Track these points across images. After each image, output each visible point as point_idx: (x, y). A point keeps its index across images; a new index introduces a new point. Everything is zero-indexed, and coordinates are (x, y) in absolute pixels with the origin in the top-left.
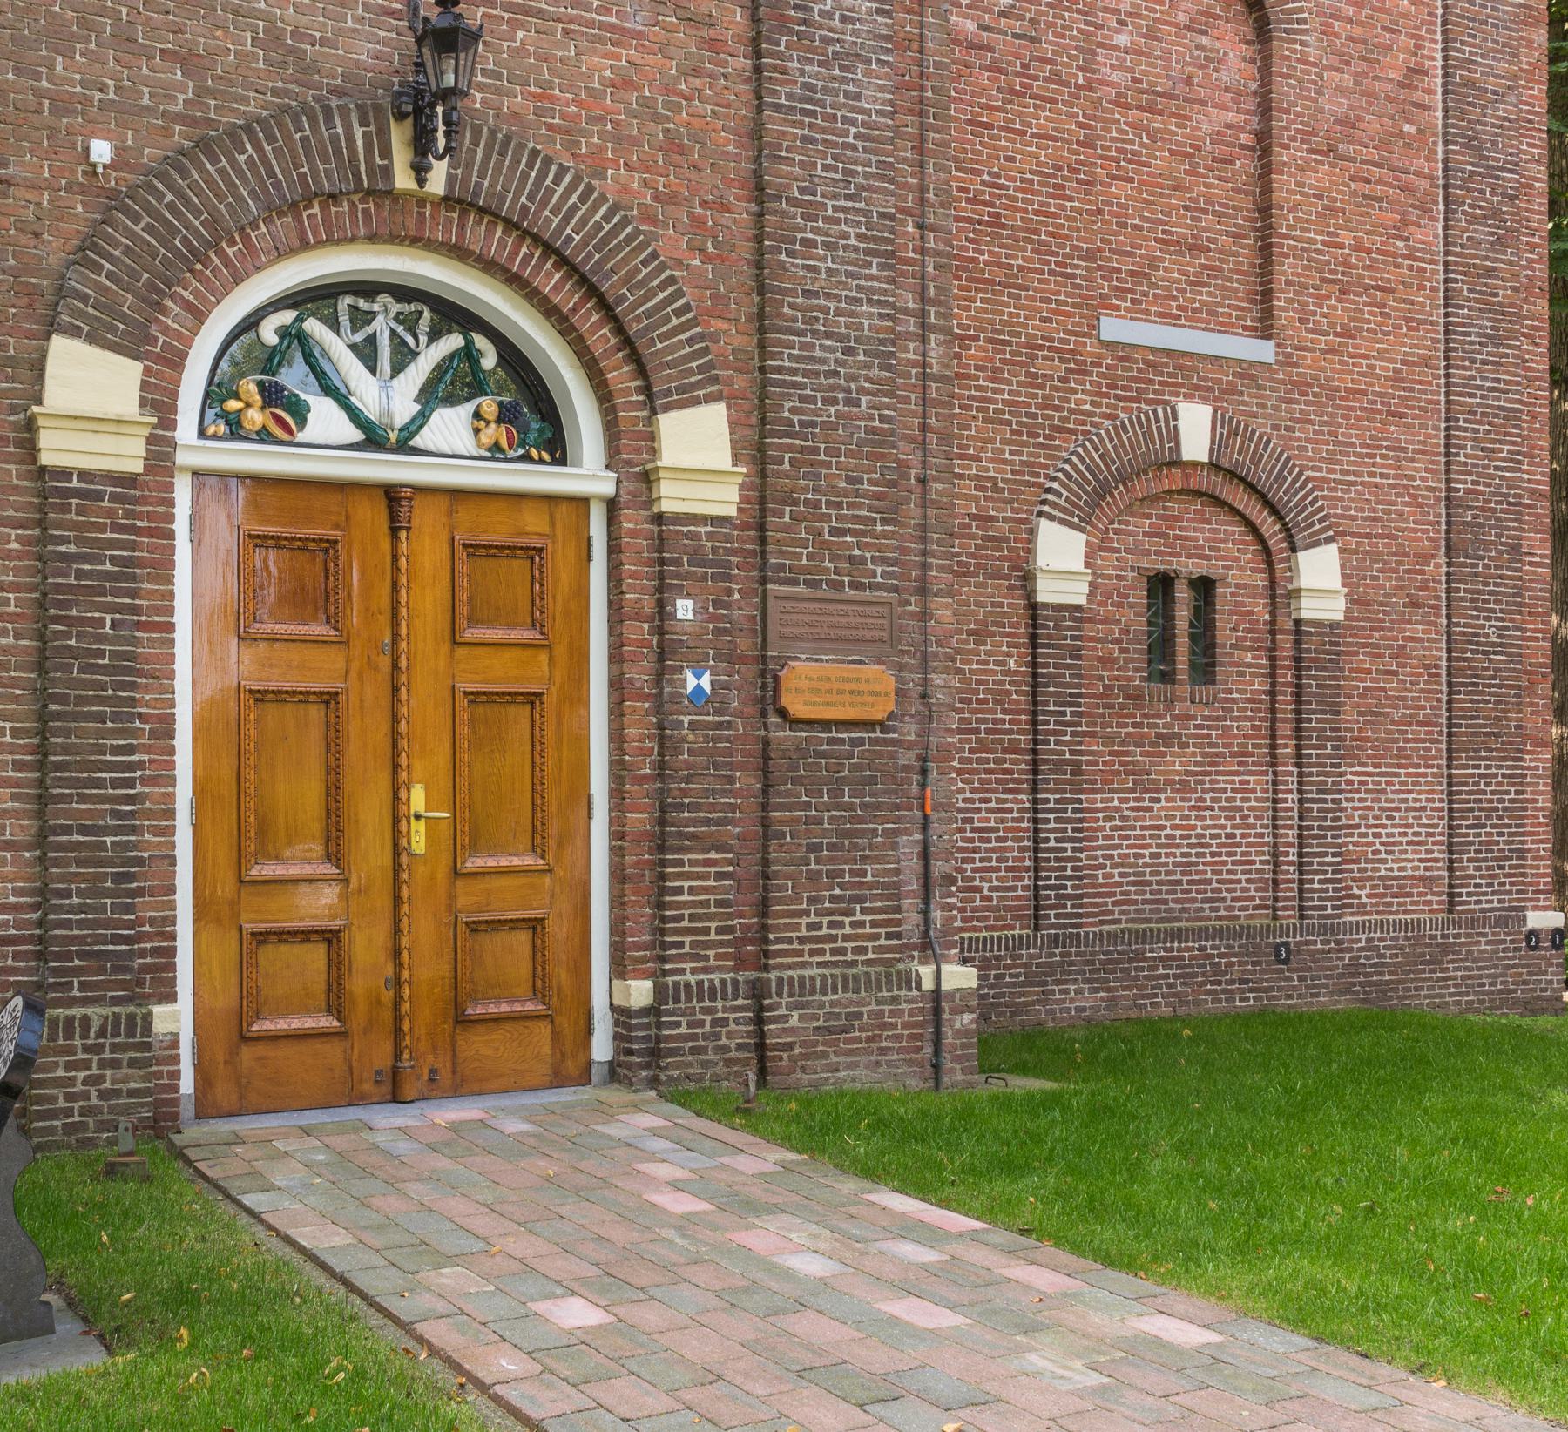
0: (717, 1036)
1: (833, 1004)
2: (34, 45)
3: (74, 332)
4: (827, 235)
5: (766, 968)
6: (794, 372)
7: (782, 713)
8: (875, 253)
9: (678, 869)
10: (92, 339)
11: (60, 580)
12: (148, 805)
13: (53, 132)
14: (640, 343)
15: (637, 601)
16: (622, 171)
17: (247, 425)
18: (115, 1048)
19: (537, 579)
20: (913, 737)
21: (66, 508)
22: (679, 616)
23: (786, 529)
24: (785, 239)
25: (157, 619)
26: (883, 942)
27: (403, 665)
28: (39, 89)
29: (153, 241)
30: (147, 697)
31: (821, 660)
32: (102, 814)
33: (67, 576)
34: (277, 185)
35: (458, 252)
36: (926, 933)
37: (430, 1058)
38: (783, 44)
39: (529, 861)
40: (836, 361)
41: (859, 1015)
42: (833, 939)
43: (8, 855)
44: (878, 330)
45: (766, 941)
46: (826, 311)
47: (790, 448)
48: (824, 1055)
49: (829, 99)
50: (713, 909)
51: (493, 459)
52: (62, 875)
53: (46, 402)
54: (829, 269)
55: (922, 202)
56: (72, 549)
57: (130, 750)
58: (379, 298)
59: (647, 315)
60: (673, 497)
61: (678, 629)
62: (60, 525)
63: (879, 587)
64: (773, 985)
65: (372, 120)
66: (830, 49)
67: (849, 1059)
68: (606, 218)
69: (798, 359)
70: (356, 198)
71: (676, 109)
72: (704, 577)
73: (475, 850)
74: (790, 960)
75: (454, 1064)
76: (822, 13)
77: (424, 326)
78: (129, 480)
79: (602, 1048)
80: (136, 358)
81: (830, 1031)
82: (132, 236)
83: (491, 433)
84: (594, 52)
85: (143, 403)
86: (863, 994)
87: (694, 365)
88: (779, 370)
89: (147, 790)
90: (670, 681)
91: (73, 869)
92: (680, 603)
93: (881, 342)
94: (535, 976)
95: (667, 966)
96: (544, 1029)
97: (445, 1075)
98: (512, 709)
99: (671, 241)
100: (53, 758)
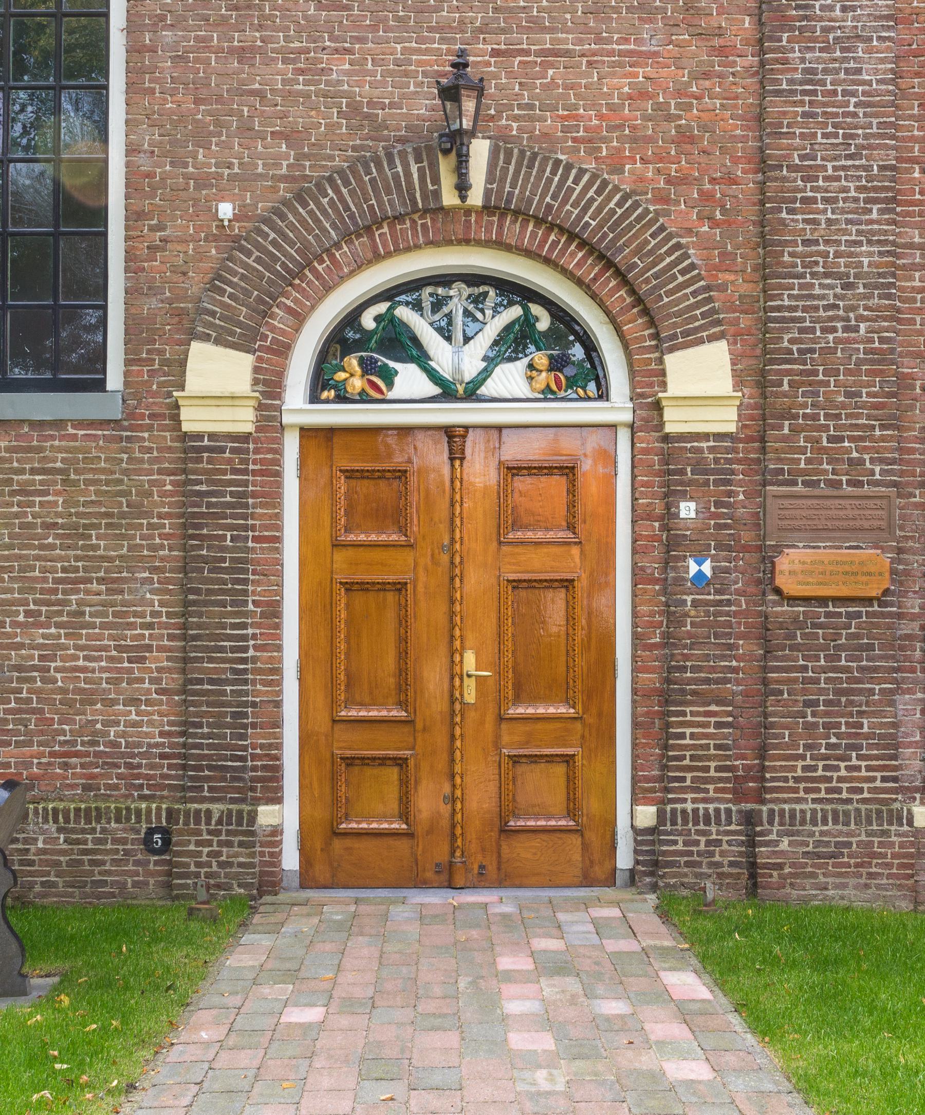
0: (711, 854)
1: (822, 833)
2: (184, 144)
3: (206, 338)
4: (827, 191)
5: (763, 802)
7: (778, 591)
8: (875, 201)
9: (681, 719)
10: (218, 342)
12: (259, 665)
13: (196, 201)
14: (649, 301)
15: (649, 504)
17: (349, 389)
18: (229, 833)
20: (917, 610)
21: (199, 460)
22: (682, 515)
23: (784, 439)
24: (784, 200)
25: (266, 534)
26: (878, 784)
28: (186, 173)
30: (259, 589)
31: (819, 547)
32: (224, 671)
33: (200, 506)
34: (352, 217)
35: (501, 245)
37: (480, 857)
40: (835, 296)
41: (848, 845)
42: (829, 780)
43: (164, 698)
45: (763, 779)
46: (825, 255)
47: (788, 373)
48: (813, 875)
50: (712, 752)
51: (545, 400)
52: (197, 712)
56: (204, 488)
57: (244, 626)
58: (453, 286)
59: (656, 276)
61: (681, 526)
63: (877, 483)
64: (765, 815)
65: (425, 157)
66: (831, 36)
67: (838, 881)
68: (619, 204)
70: (416, 217)
71: (688, 107)
72: (706, 483)
73: (518, 699)
74: (785, 796)
76: (823, 8)
77: (489, 303)
79: (624, 859)
81: (819, 856)
82: (246, 266)
83: (543, 378)
84: (613, 75)
85: (256, 382)
86: (853, 827)
87: (698, 312)
88: (779, 309)
89: (258, 654)
90: (675, 569)
91: (204, 708)
92: (683, 505)
93: (880, 275)
94: (568, 799)
95: (670, 796)
96: (576, 840)
97: (492, 868)
98: (550, 594)
100: (191, 632)
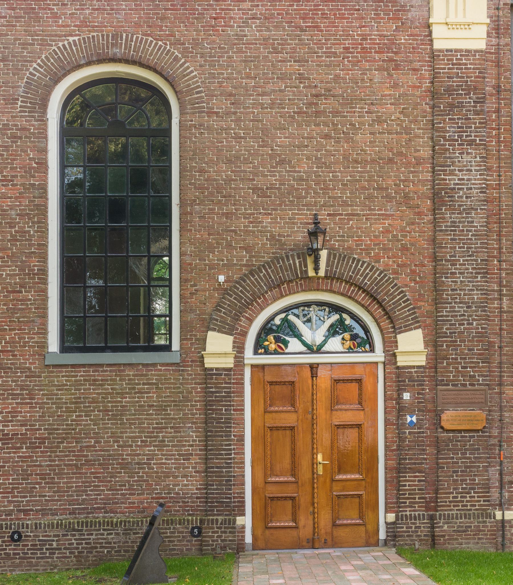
0: (417, 532)
1: (460, 523)
3: (214, 330)
4: (460, 270)
5: (437, 511)
6: (448, 316)
7: (442, 428)
9: (404, 479)
10: (219, 331)
11: (211, 399)
12: (236, 460)
13: (209, 275)
14: (391, 313)
15: (391, 394)
16: (386, 259)
17: (270, 349)
18: (225, 528)
19: (360, 389)
20: (496, 434)
21: (212, 379)
23: (444, 367)
24: (444, 273)
26: (482, 503)
27: (315, 417)
29: (236, 302)
31: (458, 410)
35: (331, 291)
36: (501, 501)
38: (443, 209)
39: (357, 476)
40: (464, 311)
41: (471, 527)
44: (480, 299)
45: (437, 502)
46: (460, 295)
47: (446, 341)
48: (457, 539)
49: (461, 225)
50: (417, 491)
51: (349, 352)
53: (206, 350)
54: (461, 281)
55: (500, 253)
56: (214, 390)
57: (230, 445)
59: (393, 304)
60: (402, 361)
61: (404, 403)
62: (210, 384)
65: (301, 257)
66: (462, 209)
67: (466, 541)
68: (379, 275)
69: (449, 312)
70: (298, 280)
74: (446, 508)
75: (332, 538)
76: (458, 197)
78: (230, 370)
79: (382, 535)
80: (231, 335)
81: (459, 531)
83: (348, 344)
84: (376, 223)
85: (234, 347)
86: (472, 520)
90: (401, 419)
91: (214, 478)
92: (405, 394)
93: (481, 303)
96: (363, 528)
99: (404, 278)
